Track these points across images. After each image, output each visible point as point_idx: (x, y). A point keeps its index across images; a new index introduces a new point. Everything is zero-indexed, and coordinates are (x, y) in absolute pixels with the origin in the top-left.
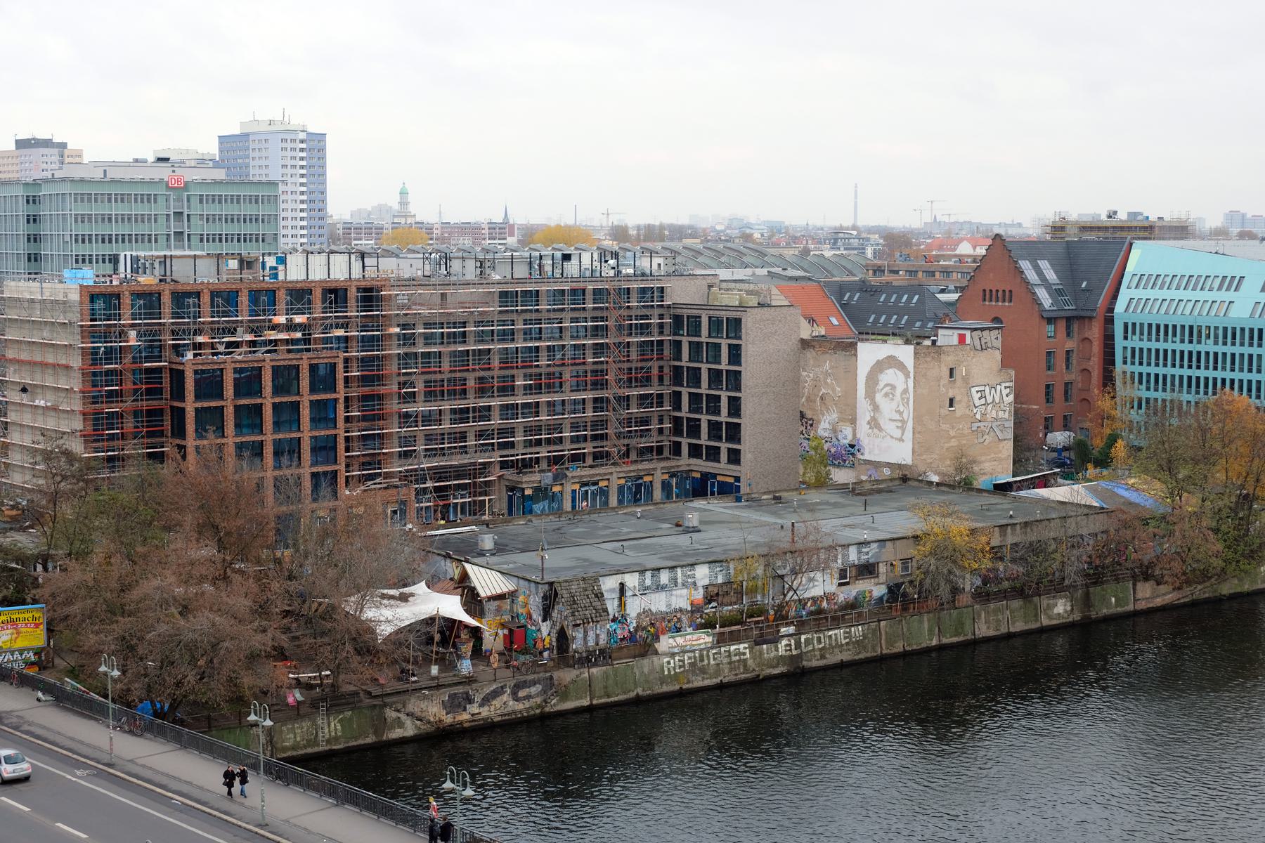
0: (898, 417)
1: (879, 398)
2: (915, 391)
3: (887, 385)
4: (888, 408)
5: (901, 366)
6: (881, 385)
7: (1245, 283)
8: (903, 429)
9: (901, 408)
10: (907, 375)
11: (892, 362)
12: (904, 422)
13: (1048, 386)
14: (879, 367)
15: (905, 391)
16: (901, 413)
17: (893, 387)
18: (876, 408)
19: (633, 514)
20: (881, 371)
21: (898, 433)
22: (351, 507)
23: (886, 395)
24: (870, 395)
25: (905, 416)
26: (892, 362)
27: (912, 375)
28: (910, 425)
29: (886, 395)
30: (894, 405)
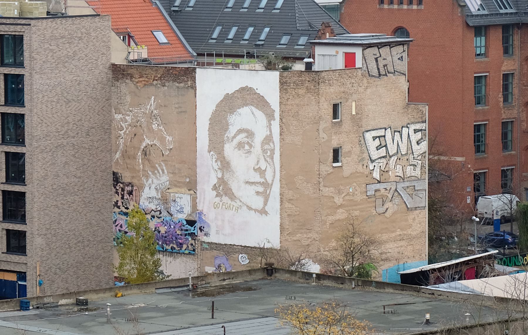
0: (257, 178)
2: (282, 140)
3: (240, 131)
4: (242, 164)
5: (261, 103)
6: (232, 130)
9: (263, 165)
10: (270, 116)
12: (267, 185)
14: (230, 103)
15: (268, 139)
16: (262, 172)
18: (225, 165)
20: (232, 110)
21: (258, 202)
23: (240, 146)
24: (217, 145)
25: (269, 176)
26: (247, 96)
27: (277, 115)
28: (276, 189)
29: (240, 146)
30: (252, 161)
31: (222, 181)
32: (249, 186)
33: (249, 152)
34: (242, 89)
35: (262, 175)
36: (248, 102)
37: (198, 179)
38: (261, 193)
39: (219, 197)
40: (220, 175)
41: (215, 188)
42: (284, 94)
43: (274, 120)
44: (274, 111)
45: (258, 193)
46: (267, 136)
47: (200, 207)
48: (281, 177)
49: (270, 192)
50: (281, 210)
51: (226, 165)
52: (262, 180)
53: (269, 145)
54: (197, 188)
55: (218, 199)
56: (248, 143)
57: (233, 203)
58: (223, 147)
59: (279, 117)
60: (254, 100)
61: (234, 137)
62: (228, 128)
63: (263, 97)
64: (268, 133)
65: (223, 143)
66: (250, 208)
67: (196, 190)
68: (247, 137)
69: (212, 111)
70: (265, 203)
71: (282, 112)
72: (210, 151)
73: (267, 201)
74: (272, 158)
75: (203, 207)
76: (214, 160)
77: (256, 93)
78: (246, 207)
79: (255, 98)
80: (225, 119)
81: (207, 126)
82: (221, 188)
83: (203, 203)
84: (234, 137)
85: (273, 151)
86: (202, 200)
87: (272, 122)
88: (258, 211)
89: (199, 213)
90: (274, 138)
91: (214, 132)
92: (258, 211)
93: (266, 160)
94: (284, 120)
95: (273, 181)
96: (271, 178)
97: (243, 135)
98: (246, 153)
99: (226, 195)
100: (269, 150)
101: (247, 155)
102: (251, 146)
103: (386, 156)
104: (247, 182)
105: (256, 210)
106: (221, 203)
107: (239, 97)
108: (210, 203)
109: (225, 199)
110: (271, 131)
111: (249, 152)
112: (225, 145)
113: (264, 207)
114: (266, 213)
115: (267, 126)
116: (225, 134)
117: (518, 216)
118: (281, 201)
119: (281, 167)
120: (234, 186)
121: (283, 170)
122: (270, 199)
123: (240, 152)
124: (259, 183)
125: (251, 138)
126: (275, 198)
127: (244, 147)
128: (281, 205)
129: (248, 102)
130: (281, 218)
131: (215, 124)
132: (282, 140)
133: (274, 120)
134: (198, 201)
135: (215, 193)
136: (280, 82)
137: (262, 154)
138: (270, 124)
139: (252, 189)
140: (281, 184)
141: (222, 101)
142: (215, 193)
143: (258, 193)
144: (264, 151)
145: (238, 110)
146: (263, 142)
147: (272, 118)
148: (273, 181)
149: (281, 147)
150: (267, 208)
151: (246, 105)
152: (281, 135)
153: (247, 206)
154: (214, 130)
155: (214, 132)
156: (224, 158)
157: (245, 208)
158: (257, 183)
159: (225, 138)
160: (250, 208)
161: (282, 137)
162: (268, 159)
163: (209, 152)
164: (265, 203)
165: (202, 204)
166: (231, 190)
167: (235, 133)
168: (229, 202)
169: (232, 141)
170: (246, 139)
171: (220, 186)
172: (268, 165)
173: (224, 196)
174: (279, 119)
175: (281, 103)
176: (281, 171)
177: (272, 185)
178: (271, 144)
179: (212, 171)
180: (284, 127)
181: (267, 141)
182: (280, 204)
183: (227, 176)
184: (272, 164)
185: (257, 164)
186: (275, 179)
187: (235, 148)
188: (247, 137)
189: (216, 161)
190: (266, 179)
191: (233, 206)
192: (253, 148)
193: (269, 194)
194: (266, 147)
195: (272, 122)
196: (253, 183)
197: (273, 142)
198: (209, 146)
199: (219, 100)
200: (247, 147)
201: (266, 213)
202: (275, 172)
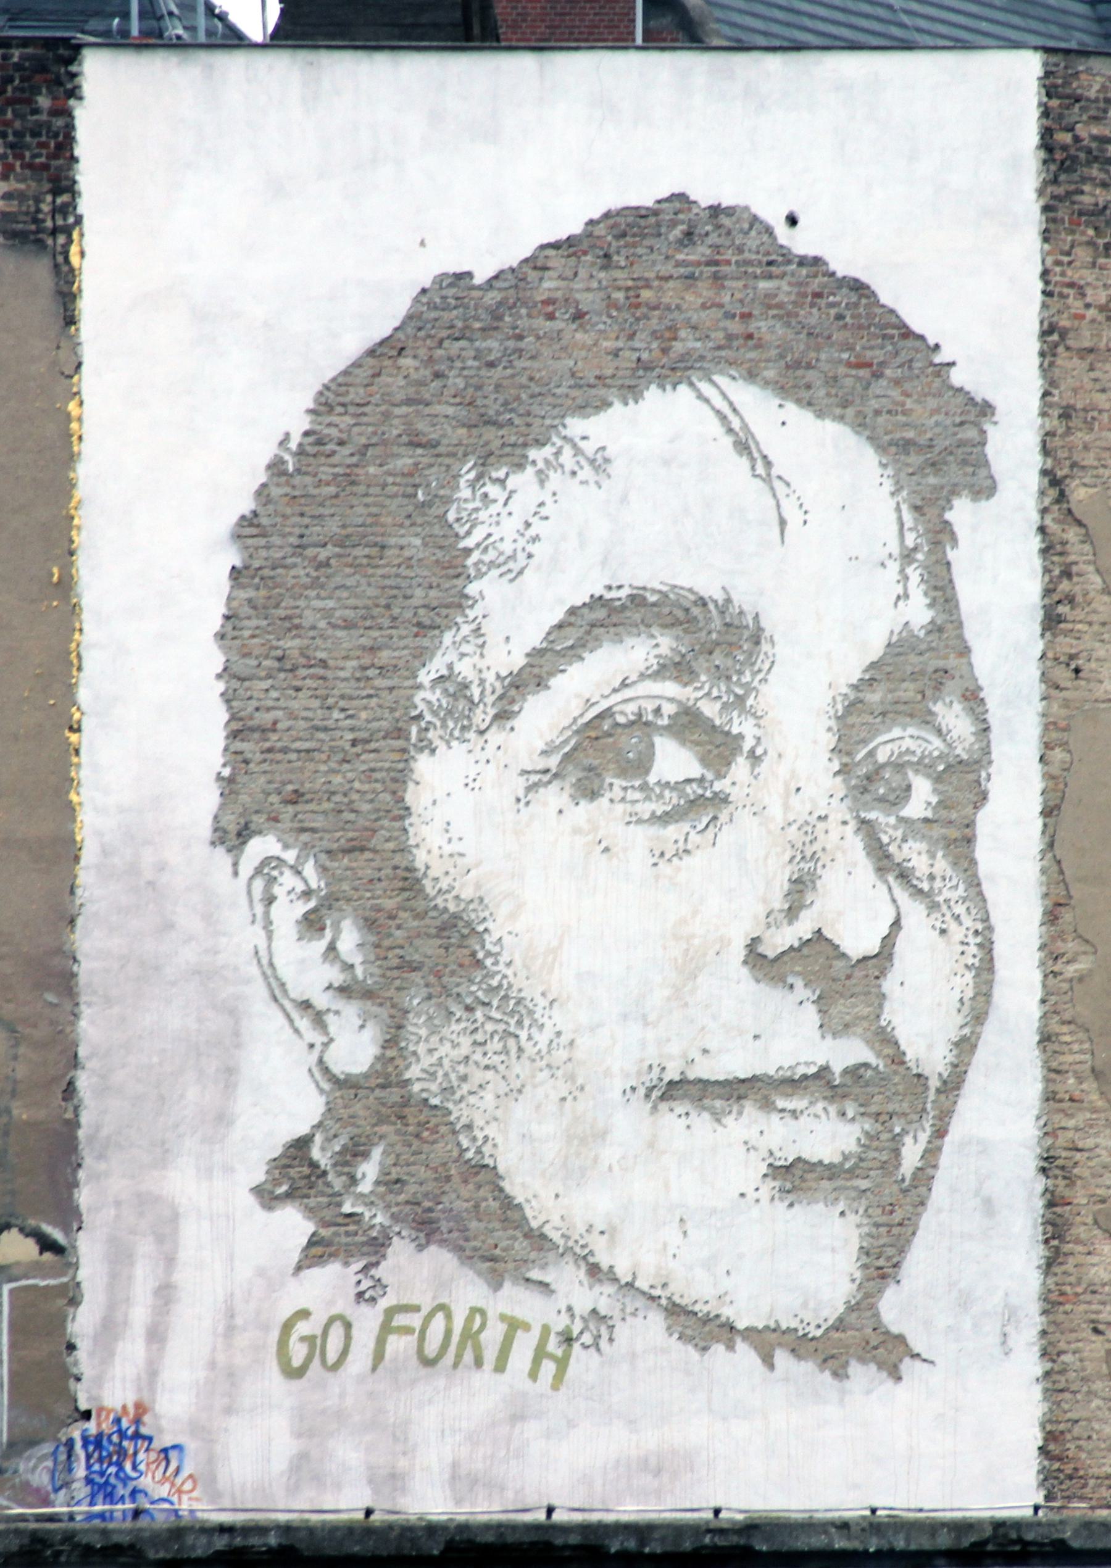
0: (794, 1035)
1: (471, 811)
2: (1064, 671)
3: (600, 619)
4: (613, 929)
5: (838, 342)
6: (509, 617)
7: (485, 593)
8: (890, 1209)
9: (854, 910)
10: (936, 453)
11: (679, 290)
12: (899, 1099)
13: (932, 1362)
14: (470, 370)
15: (922, 670)
16: (848, 984)
17: (713, 637)
18: (421, 948)
19: (807, 1064)
20: (509, 431)
21: (810, 1262)
22: (337, 496)
23: (598, 755)
24: (317, 757)
25: (921, 1012)
26: (679, 290)
27: (1015, 448)
28: (1001, 1119)
29: (598, 755)
30: (730, 884)
31: (382, 1108)
32: (702, 1122)
33: (696, 804)
34: (623, 234)
35: (839, 1008)
36: (688, 342)
37: (95, 1113)
38: (831, 1171)
39: (346, 1255)
40: (355, 1048)
41: (295, 1175)
42: (1083, 254)
43: (985, 489)
44: (986, 409)
45: (793, 1177)
46: (901, 647)
47: (109, 1383)
48: (1052, 1002)
49: (932, 1154)
50: (1052, 1302)
51: (430, 948)
52: (847, 1053)
53: (927, 719)
54: (84, 1197)
55: (328, 1286)
56: (688, 724)
57: (514, 1300)
58: (400, 777)
59: (1037, 460)
60: (761, 326)
61: (531, 677)
62: (461, 602)
63: (858, 287)
64: (918, 612)
65: (395, 744)
66: (701, 1327)
67: (70, 1216)
68: (677, 668)
69: (267, 452)
70: (881, 1264)
71: (1063, 416)
72: (244, 834)
73: (902, 1246)
74: (959, 842)
75: (152, 1372)
76: (288, 913)
77: (778, 260)
78: (656, 1321)
79: (769, 302)
80: (429, 513)
81: (208, 596)
82: (369, 1171)
83: (156, 1336)
84: (531, 677)
85: (965, 780)
86: (140, 1314)
87: (962, 513)
88: (800, 1344)
89: (96, 1442)
90: (976, 658)
91: (291, 644)
92: (800, 1344)
93: (884, 862)
94: (1079, 493)
95: (965, 1046)
96: (951, 1026)
97: (635, 653)
98: (664, 819)
99: (427, 1229)
100: (924, 766)
101: (673, 832)
102: (718, 747)
103: (557, 459)
104: (676, 1090)
105: (768, 1341)
106: (367, 1321)
107: (588, 300)
108: (230, 1330)
109: (417, 1271)
110: (942, 591)
111: (701, 805)
112: (423, 764)
113: (863, 1304)
114: (890, 1353)
115: (908, 556)
116: (422, 656)
117: (867, 1127)
118: (1056, 1231)
119: (1051, 917)
120: (523, 1141)
121: (1071, 946)
122: (928, 1221)
123: (607, 813)
124: (819, 1082)
125: (721, 675)
126: (988, 1207)
127: (642, 765)
128: (1050, 1265)
129: (688, 342)
130: (1056, 1383)
131: (302, 572)
132: (1063, 675)
133: (985, 489)
134: (83, 1323)
135: (293, 1226)
136: (1047, 143)
137: (840, 811)
138: (942, 534)
139: (732, 1150)
140: (1053, 1072)
141: (386, 351)
142: (293, 1226)
143: (793, 1177)
144: (870, 785)
145: (576, 426)
146: (853, 706)
147: (954, 472)
148: (965, 1046)
149: (1055, 736)
150: (893, 1309)
151: (675, 370)
152: (1051, 622)
153: (675, 1311)
154: (295, 629)
155: (291, 644)
156: (409, 881)
157: (652, 1327)
158: (792, 1084)
159: (426, 697)
160: (701, 1327)
161: (1066, 645)
162: (916, 855)
163: (232, 835)
164: (881, 1264)
165: (132, 1351)
166: (483, 1173)
167: (535, 639)
168: (468, 1291)
169: (503, 716)
170: (670, 688)
171: (356, 1152)
172: (914, 913)
173: (400, 1251)
174: (1033, 481)
175: (1053, 337)
176: (1052, 956)
177: (953, 1084)
178: (954, 718)
179: (267, 1025)
180: (1078, 551)
181: (908, 690)
182: (1037, 1254)
183: (438, 1051)
184: (952, 891)
185: (792, 913)
186: (990, 1033)
187: (538, 780)
188: (677, 668)
189: (312, 924)
190: (885, 1039)
191: (514, 1326)
192: (740, 768)
193: (924, 1176)
194: (896, 741)
195: (962, 513)
196: (738, 1091)
197: (973, 698)
198: (229, 786)
199: (352, 344)
200: (674, 761)
201: (890, 1353)
202: (985, 969)
